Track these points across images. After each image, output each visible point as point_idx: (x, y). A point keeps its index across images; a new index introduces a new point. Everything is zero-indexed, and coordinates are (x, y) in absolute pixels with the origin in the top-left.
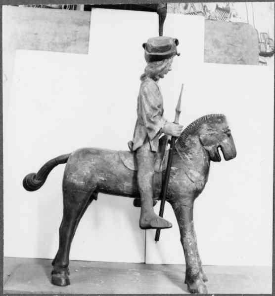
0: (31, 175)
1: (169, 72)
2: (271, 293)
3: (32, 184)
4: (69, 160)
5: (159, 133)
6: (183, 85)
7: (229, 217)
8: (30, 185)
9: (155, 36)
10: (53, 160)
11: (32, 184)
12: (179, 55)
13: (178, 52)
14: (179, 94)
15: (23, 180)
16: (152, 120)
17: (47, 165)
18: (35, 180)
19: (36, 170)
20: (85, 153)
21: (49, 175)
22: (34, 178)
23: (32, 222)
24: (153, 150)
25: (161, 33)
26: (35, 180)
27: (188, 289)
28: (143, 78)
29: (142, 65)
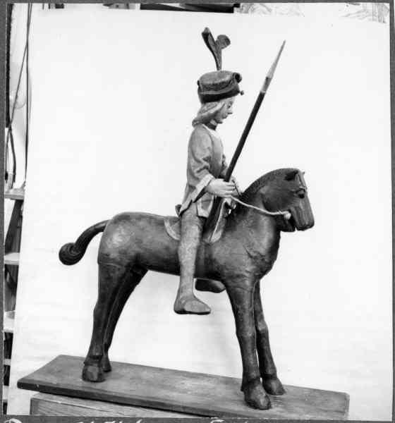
0: (67, 246)
1: (230, 115)
2: (391, 420)
3: (71, 255)
4: (205, 156)
5: (203, 193)
6: (284, 42)
7: (320, 306)
8: (66, 258)
9: (210, 71)
10: (91, 227)
11: (71, 255)
12: (242, 94)
13: (241, 90)
14: (31, 26)
15: (58, 253)
16: (196, 175)
17: (85, 234)
18: (72, 252)
19: (74, 240)
20: (123, 219)
21: (92, 241)
22: (70, 250)
23: (52, 314)
24: (200, 215)
25: (218, 67)
26: (72, 252)
27: (246, 400)
28: (196, 123)
29: (194, 106)
